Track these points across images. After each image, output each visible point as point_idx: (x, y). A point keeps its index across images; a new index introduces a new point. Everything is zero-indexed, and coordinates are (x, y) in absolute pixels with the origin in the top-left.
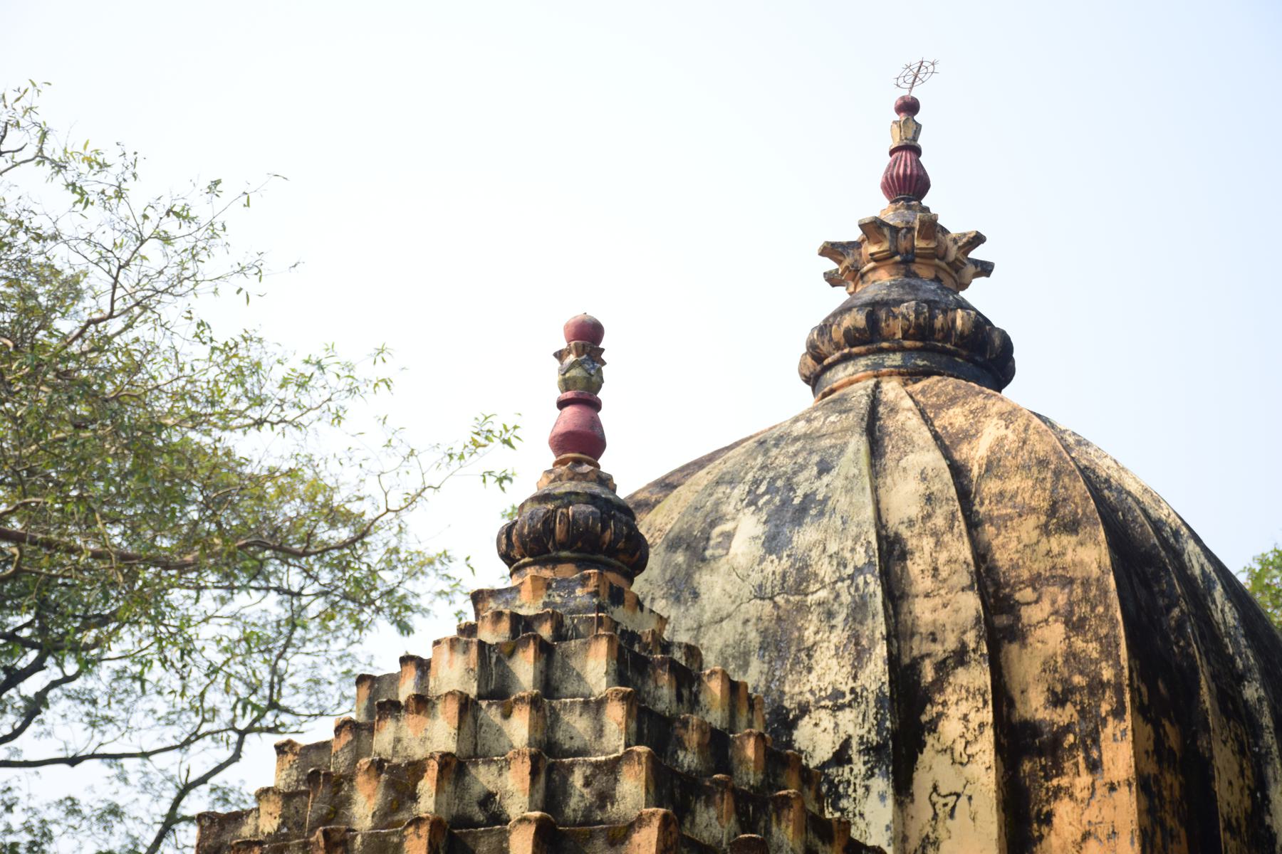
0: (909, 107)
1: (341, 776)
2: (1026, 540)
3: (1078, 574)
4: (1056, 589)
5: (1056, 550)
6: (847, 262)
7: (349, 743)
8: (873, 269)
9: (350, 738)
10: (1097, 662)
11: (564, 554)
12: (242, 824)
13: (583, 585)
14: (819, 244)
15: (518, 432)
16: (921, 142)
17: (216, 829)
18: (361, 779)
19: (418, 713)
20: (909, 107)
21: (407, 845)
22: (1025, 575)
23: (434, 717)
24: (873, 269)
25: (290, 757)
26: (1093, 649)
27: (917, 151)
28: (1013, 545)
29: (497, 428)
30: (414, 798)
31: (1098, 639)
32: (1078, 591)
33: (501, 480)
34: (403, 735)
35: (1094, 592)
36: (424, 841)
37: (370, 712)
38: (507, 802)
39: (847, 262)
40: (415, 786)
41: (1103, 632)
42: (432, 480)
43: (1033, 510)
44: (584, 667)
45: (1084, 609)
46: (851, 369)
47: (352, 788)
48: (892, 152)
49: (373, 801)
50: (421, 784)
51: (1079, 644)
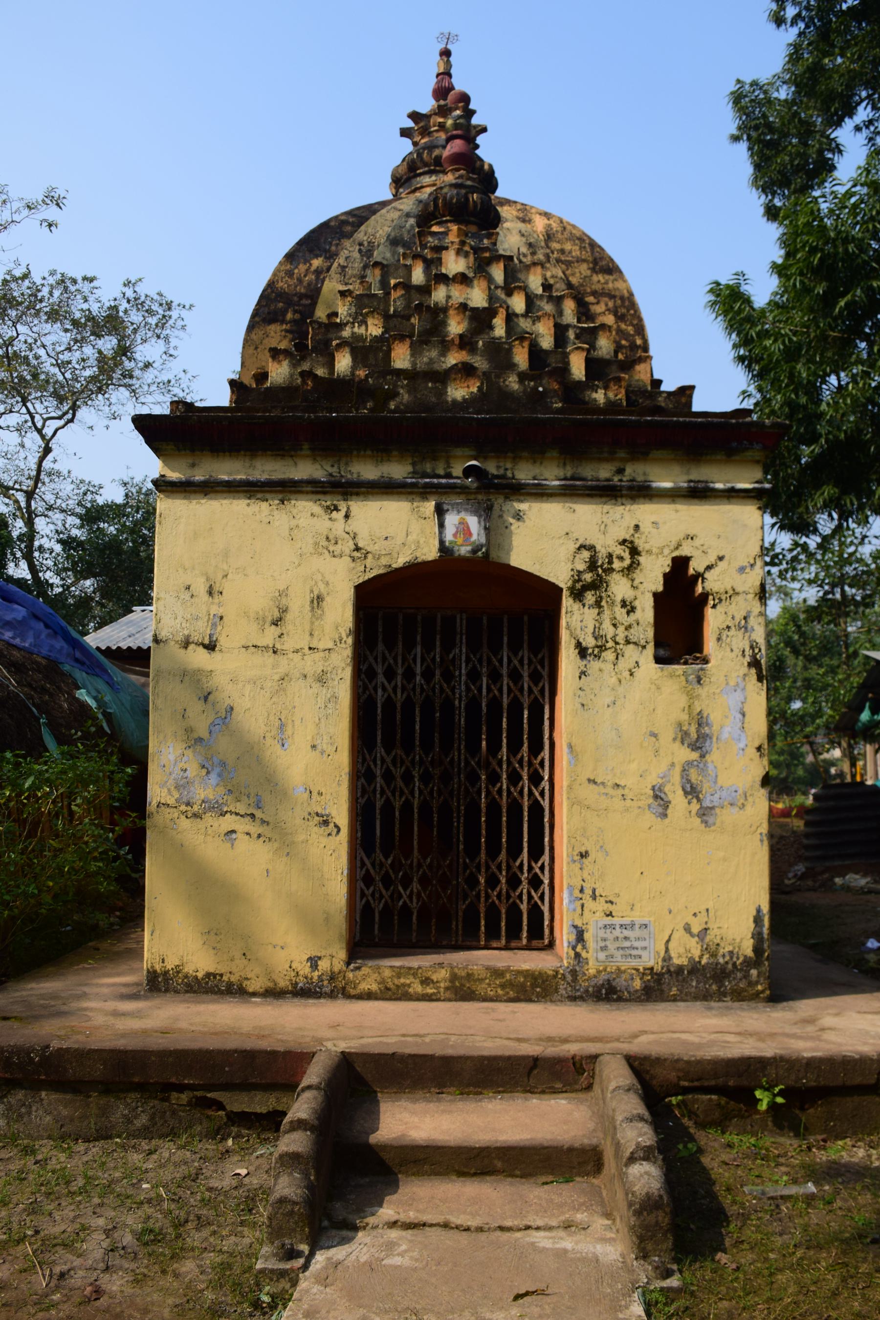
0: (446, 53)
1: (119, 345)
2: (584, 274)
3: (617, 293)
5: (602, 281)
7: (402, 295)
9: (403, 292)
10: (633, 336)
12: (342, 330)
15: (64, 201)
16: (452, 71)
17: (323, 330)
18: (452, 312)
20: (446, 53)
21: (515, 350)
22: (589, 290)
23: (472, 287)
25: (349, 299)
26: (630, 330)
27: (450, 76)
30: (491, 328)
31: (633, 325)
32: (619, 302)
33: (50, 225)
34: (452, 294)
35: (627, 303)
36: (526, 350)
38: (540, 340)
41: (635, 322)
42: (16, 217)
43: (584, 261)
44: (527, 278)
45: (624, 311)
46: (434, 178)
47: (446, 316)
48: (438, 75)
49: (462, 326)
50: (495, 321)
51: (623, 326)
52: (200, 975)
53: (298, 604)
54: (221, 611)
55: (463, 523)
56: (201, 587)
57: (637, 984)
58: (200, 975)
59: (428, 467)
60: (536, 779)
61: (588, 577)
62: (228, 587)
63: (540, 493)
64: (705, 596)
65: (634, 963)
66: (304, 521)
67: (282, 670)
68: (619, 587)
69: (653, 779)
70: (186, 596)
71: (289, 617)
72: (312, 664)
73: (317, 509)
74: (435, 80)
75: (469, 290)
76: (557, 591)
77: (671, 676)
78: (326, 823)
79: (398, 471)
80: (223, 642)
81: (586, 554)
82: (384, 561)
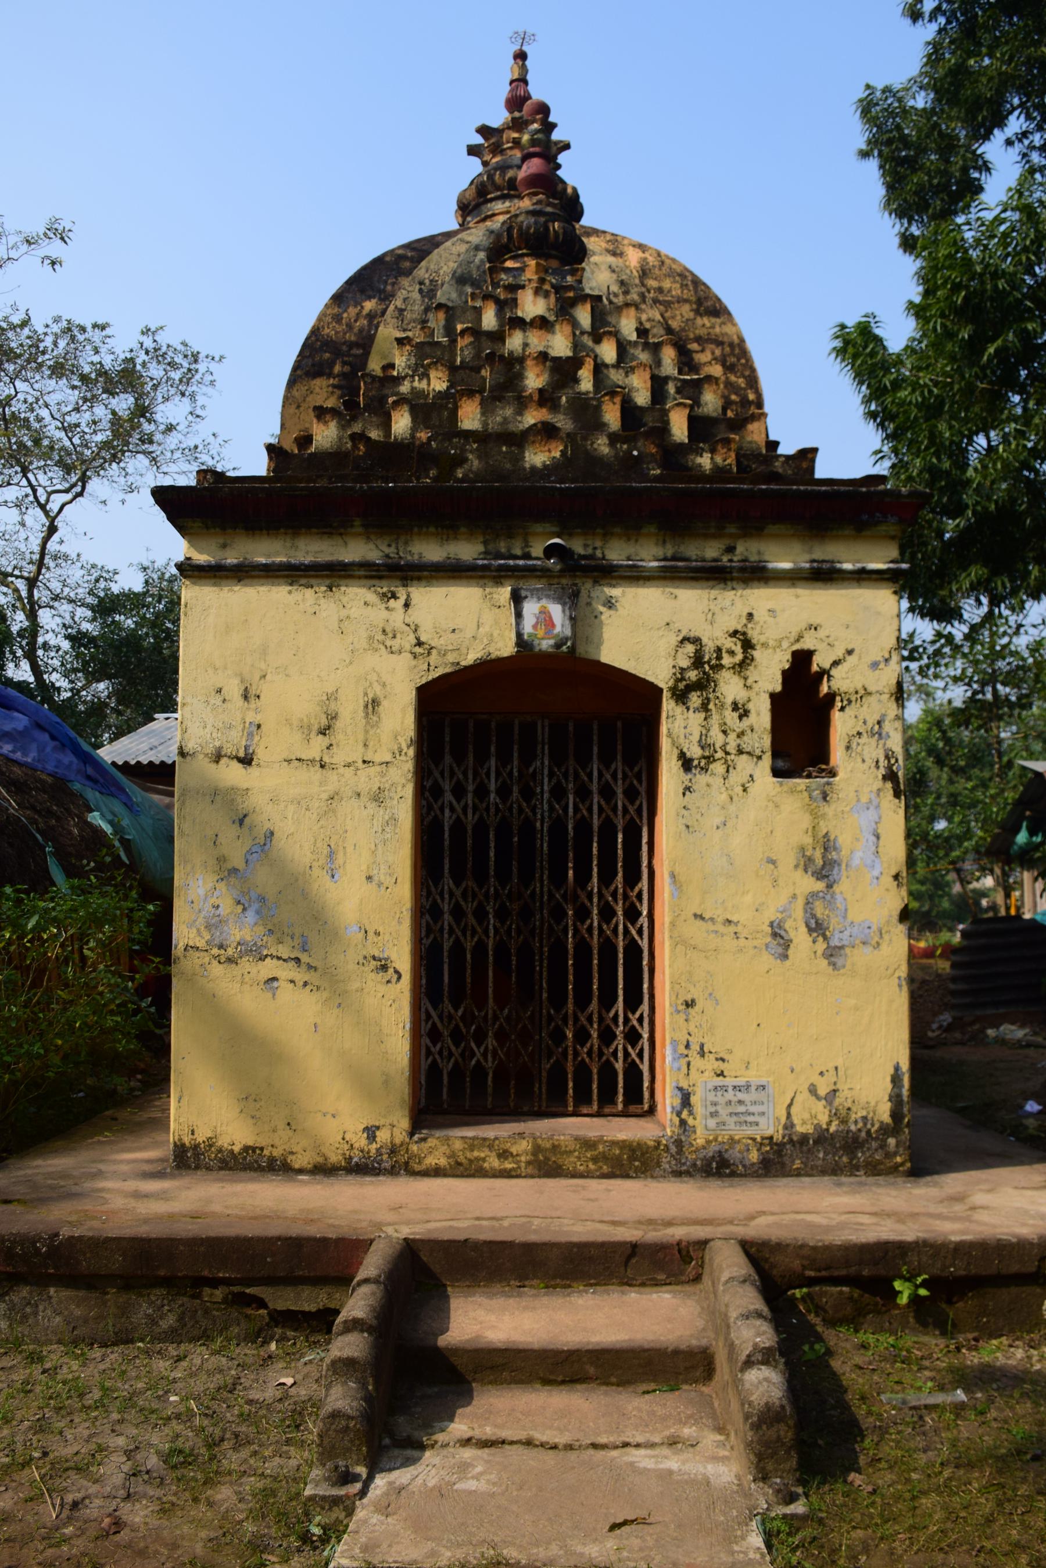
0: (521, 56)
1: (136, 404)
2: (686, 316)
4: (713, 346)
6: (493, 140)
7: (471, 343)
8: (511, 148)
9: (471, 339)
10: (745, 389)
11: (554, 252)
13: (572, 275)
14: (479, 124)
15: (70, 234)
16: (529, 77)
17: (377, 385)
19: (541, 328)
20: (521, 56)
22: (692, 336)
23: (553, 333)
24: (511, 148)
25: (408, 347)
26: (741, 382)
27: (526, 83)
28: (679, 318)
29: (61, 228)
30: (577, 381)
32: (727, 349)
33: (53, 263)
34: (529, 341)
35: (737, 351)
37: (501, 325)
38: (634, 394)
39: (493, 140)
40: (576, 373)
41: (747, 373)
42: (13, 254)
44: (618, 322)
45: (733, 360)
46: (507, 204)
47: (523, 368)
48: (512, 82)
50: (580, 373)
51: (733, 378)
52: (237, 1149)
53: (350, 709)
54: (258, 719)
55: (544, 612)
56: (233, 690)
57: (754, 1156)
58: (237, 1149)
59: (502, 546)
60: (632, 915)
61: (693, 675)
62: (266, 690)
63: (636, 576)
64: (831, 697)
65: (750, 1131)
66: (356, 610)
67: (331, 788)
68: (730, 687)
69: (771, 914)
70: (217, 700)
71: (339, 724)
72: (367, 780)
73: (371, 596)
74: (508, 88)
75: (549, 336)
76: (650, 693)
77: (792, 791)
78: (384, 968)
79: (467, 550)
80: (261, 755)
81: (690, 649)
82: (451, 658)
